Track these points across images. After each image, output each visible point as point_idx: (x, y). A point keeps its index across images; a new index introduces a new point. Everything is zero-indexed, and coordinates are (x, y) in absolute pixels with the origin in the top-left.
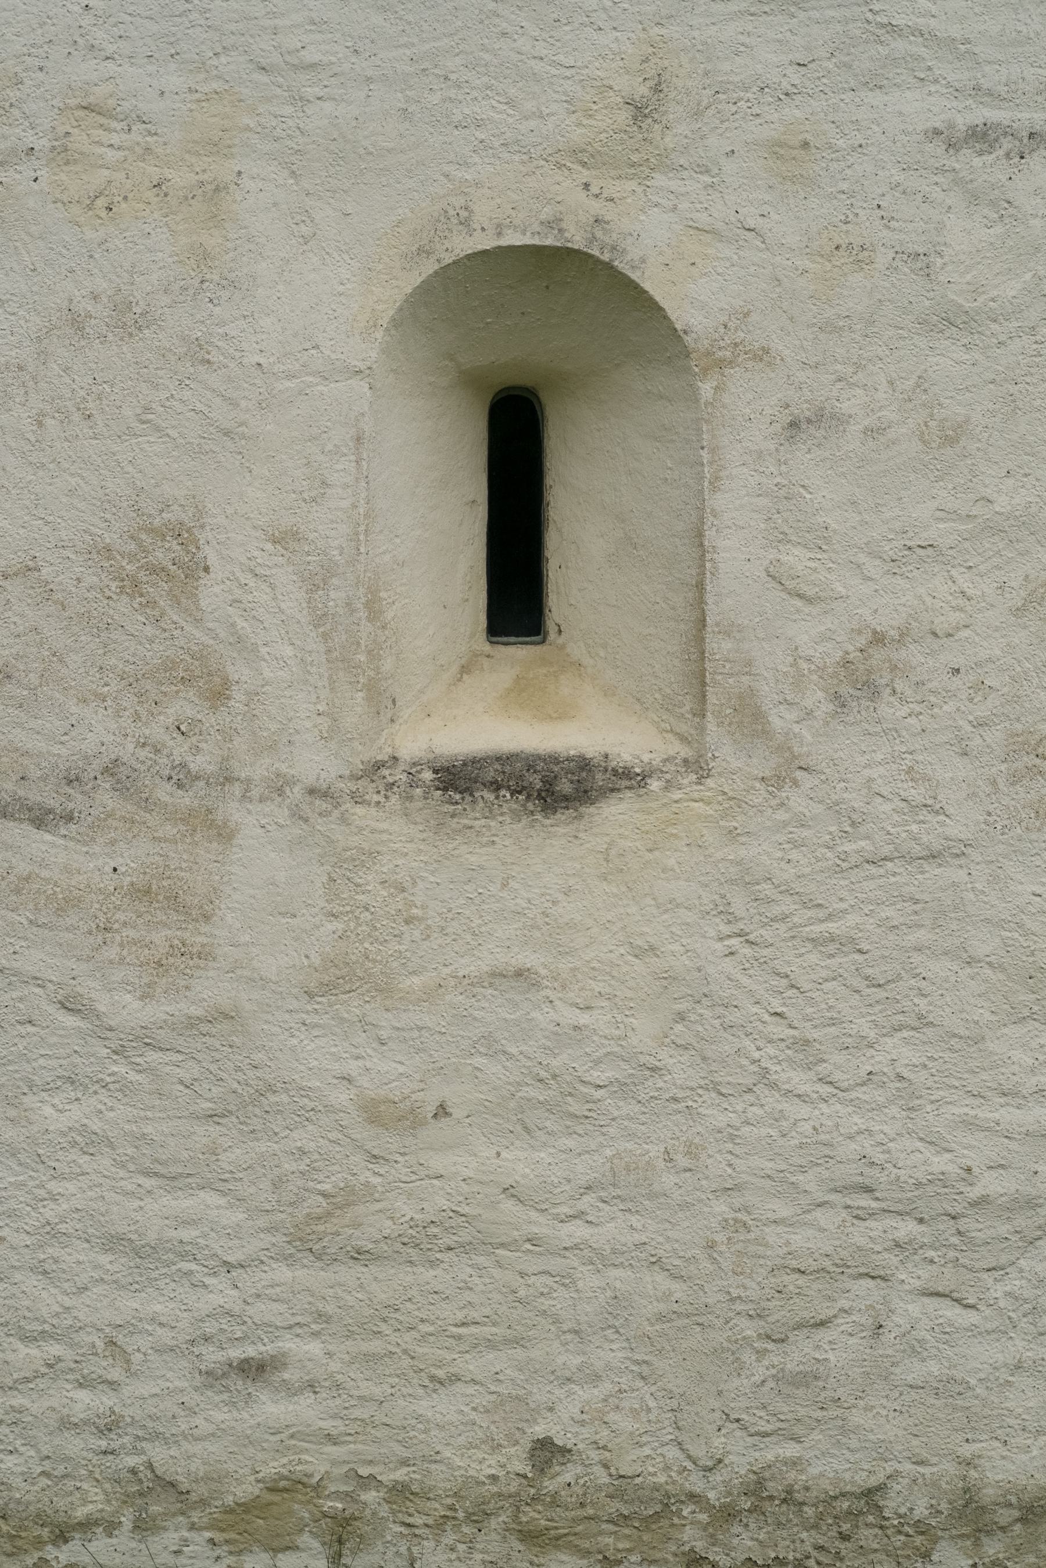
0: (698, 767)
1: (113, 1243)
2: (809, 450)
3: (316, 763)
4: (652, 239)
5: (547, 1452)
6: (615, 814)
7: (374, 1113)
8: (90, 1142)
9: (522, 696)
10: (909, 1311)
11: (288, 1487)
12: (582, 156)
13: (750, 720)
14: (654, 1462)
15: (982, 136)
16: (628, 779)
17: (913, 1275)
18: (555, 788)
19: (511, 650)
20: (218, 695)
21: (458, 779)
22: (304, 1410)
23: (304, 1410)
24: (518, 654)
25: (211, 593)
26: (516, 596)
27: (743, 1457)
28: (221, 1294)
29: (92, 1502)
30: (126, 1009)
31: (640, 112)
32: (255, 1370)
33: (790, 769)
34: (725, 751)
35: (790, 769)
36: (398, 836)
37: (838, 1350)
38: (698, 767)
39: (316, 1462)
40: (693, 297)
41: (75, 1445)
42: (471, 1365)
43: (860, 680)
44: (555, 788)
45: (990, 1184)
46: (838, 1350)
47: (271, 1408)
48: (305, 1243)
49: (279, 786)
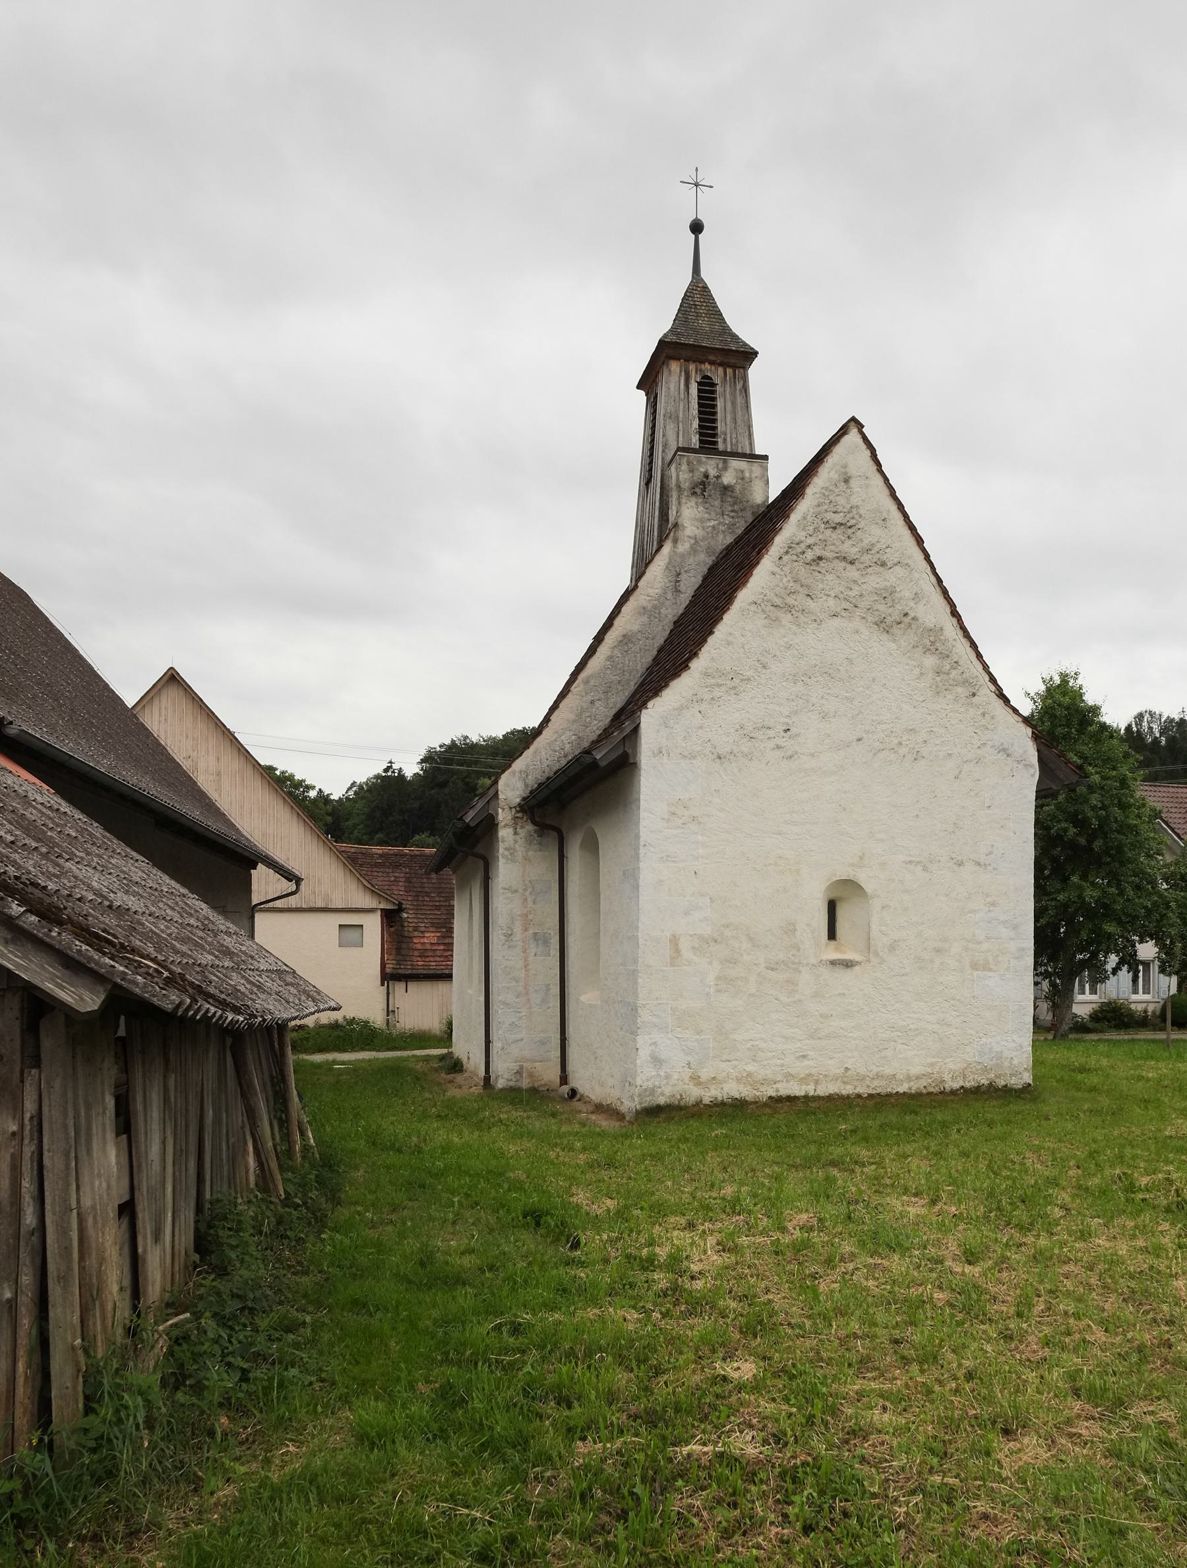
0: (869, 961)
1: (783, 1037)
2: (79, 900)
3: (813, 961)
4: (862, 878)
5: (847, 1069)
6: (856, 968)
7: (821, 1016)
8: (780, 1021)
9: (837, 949)
10: (900, 1046)
11: (810, 1075)
12: (852, 865)
13: (877, 954)
14: (862, 1071)
15: (911, 862)
16: (858, 963)
17: (900, 1041)
18: (848, 964)
19: (571, 920)
20: (798, 950)
21: (833, 963)
22: (811, 1063)
23: (811, 1063)
24: (833, 942)
25: (798, 934)
26: (832, 935)
27: (875, 1070)
28: (799, 1045)
29: (779, 1078)
30: (785, 999)
31: (861, 858)
32: (804, 1057)
33: (882, 961)
34: (874, 960)
35: (882, 961)
36: (826, 973)
37: (889, 1053)
38: (869, 961)
39: (814, 1071)
40: (869, 887)
41: (778, 1069)
42: (836, 1056)
43: (892, 947)
44: (848, 964)
45: (912, 1026)
46: (889, 1053)
47: (806, 1063)
48: (811, 1037)
49: (808, 964)
